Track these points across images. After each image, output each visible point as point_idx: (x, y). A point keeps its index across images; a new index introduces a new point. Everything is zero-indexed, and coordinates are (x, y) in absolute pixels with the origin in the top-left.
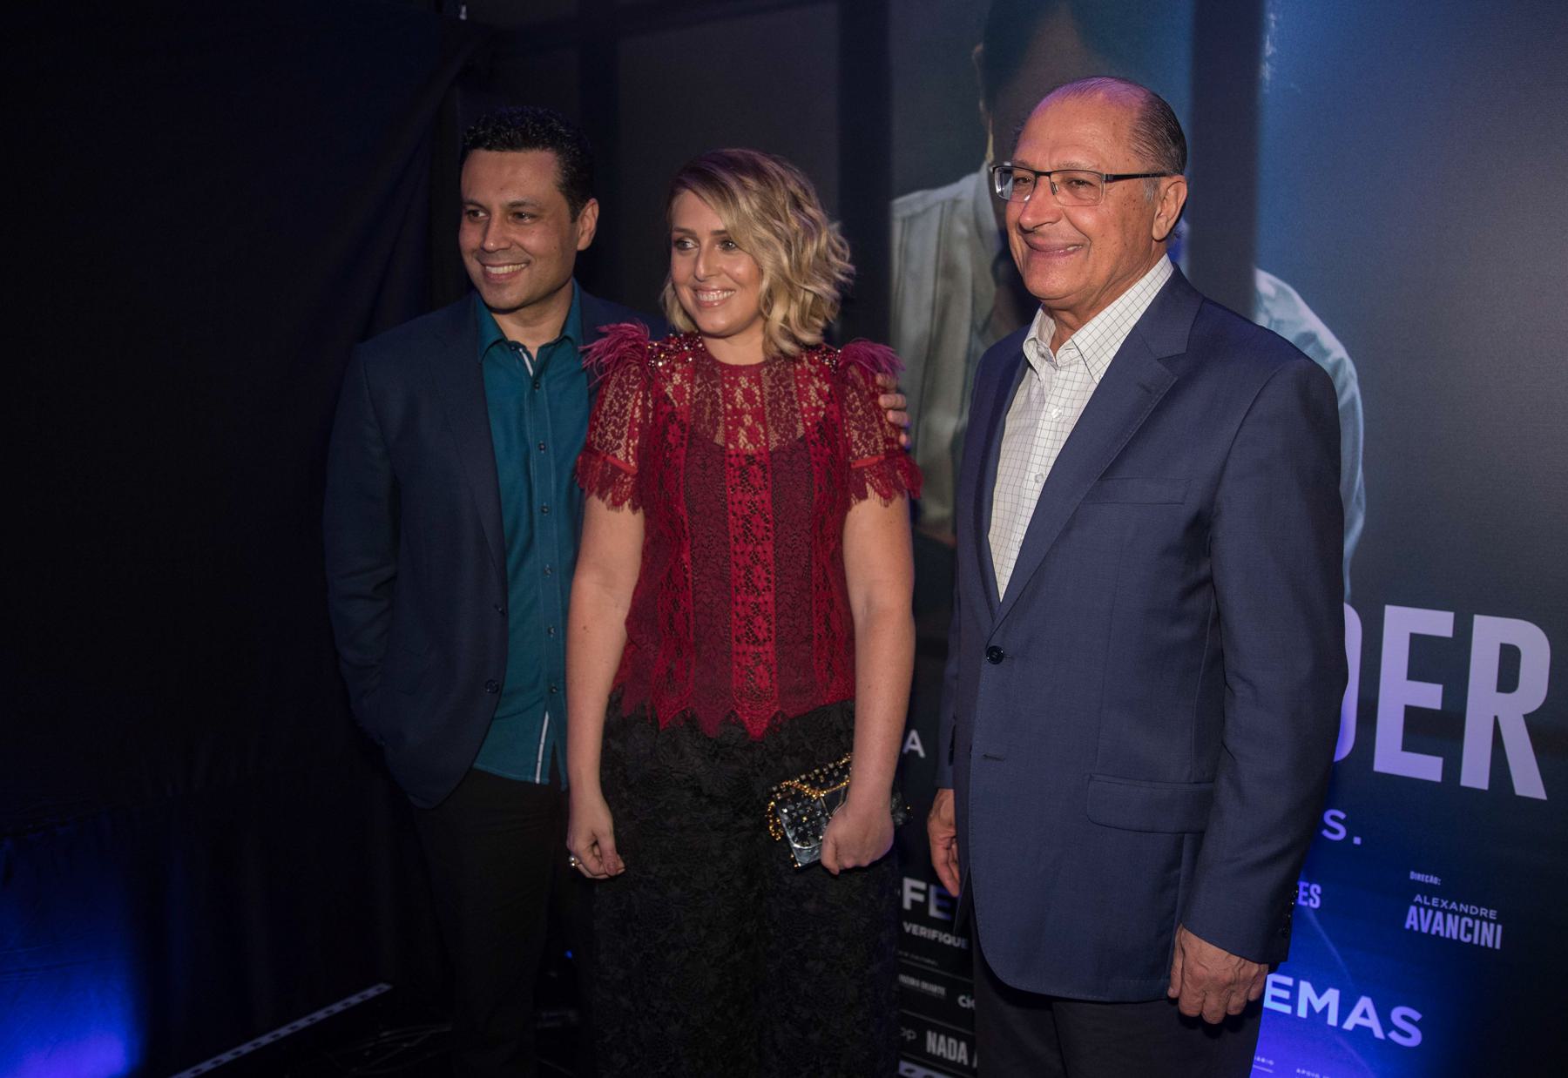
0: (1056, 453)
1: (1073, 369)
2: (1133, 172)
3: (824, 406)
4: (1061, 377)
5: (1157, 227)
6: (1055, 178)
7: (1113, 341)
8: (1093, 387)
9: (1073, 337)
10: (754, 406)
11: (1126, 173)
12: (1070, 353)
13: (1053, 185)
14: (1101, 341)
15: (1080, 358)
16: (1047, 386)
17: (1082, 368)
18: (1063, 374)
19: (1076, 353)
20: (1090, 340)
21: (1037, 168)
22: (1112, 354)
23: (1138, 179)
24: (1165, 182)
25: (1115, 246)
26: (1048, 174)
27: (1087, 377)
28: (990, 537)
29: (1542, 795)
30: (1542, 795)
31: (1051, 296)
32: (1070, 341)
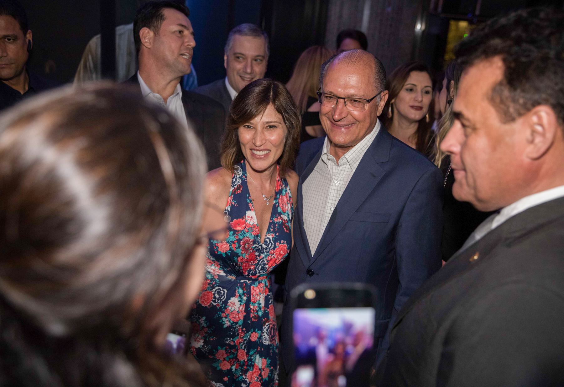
0: (338, 199)
1: (344, 166)
2: (375, 95)
3: (524, 35)
4: (347, 167)
5: (379, 111)
6: (346, 100)
7: (358, 159)
8: (352, 174)
9: (345, 155)
10: (219, 306)
11: (373, 96)
12: (344, 161)
13: (345, 102)
14: (356, 156)
15: (347, 162)
16: (331, 170)
17: (348, 166)
18: (340, 168)
19: (346, 161)
20: (352, 157)
21: (338, 95)
22: (358, 163)
23: (374, 99)
24: (382, 94)
25: (368, 124)
26: (344, 99)
27: (350, 170)
28: (304, 226)
29: (99, 36)
30: (99, 36)
31: (457, 91)
32: (344, 156)
